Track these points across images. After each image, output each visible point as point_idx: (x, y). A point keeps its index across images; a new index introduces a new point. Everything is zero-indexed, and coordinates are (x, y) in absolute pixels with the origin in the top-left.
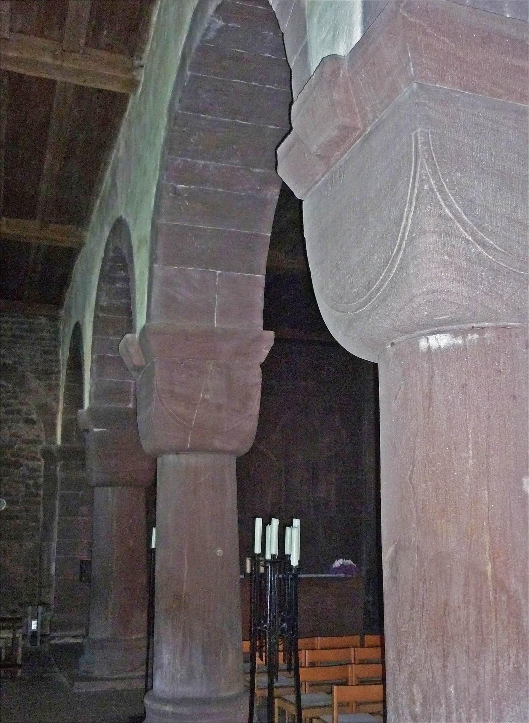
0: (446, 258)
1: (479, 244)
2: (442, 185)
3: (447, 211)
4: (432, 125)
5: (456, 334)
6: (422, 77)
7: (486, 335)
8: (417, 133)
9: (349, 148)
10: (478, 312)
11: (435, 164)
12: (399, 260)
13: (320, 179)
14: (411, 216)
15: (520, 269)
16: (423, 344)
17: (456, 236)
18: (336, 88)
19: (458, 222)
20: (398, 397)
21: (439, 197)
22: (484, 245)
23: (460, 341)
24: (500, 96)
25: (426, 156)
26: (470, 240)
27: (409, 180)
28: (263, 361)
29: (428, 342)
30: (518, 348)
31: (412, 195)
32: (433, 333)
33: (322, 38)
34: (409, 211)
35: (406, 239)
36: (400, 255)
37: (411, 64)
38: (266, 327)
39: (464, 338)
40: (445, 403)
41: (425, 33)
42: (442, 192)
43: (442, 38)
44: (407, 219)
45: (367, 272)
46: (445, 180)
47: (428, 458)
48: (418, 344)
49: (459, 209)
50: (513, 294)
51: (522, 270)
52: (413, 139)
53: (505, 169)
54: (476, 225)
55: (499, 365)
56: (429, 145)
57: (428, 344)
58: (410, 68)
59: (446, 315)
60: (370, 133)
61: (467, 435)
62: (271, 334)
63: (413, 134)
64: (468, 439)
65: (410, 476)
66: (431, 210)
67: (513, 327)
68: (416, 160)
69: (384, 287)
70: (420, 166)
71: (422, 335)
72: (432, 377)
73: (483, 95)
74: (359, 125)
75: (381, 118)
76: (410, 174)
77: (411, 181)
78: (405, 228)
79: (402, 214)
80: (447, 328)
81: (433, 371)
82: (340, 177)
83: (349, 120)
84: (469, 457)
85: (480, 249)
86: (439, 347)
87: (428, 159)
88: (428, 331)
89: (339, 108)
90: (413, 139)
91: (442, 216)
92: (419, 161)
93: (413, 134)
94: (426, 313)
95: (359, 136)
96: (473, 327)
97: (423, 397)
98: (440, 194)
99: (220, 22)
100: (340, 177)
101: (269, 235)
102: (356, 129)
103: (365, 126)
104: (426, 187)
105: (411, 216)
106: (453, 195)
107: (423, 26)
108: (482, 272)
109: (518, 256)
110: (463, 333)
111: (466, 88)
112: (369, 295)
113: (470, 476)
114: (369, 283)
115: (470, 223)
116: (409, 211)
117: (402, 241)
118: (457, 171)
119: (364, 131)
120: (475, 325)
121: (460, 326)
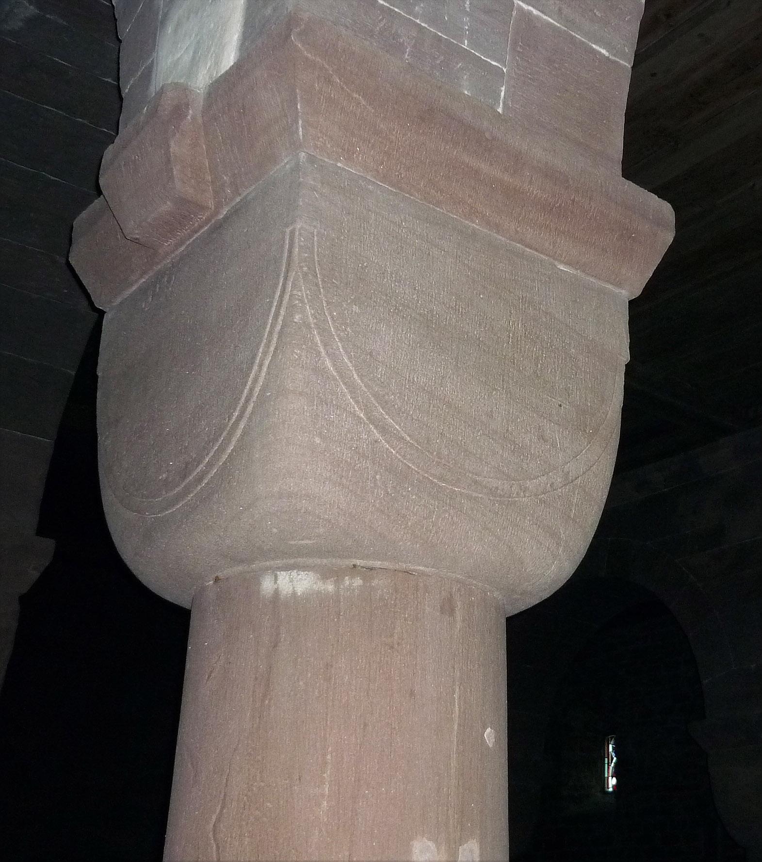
0: (318, 440)
1: (376, 427)
2: (325, 321)
3: (328, 363)
4: (321, 221)
5: (326, 574)
6: (316, 147)
7: (375, 583)
8: (294, 229)
9: (190, 236)
10: (364, 542)
11: (317, 285)
12: (239, 432)
13: (136, 281)
14: (267, 363)
15: (441, 478)
16: (267, 585)
17: (338, 407)
18: (177, 135)
19: (345, 384)
20: (213, 675)
21: (318, 339)
22: (384, 430)
23: (330, 587)
24: (438, 204)
25: (305, 269)
26: (361, 418)
27: (271, 302)
28: (24, 589)
29: (275, 583)
30: (428, 609)
31: (273, 326)
32: (288, 568)
33: (175, 58)
34: (265, 353)
35: (254, 399)
36: (242, 425)
37: (300, 122)
38: (41, 531)
39: (337, 582)
40: (292, 693)
41: (329, 81)
42: (323, 330)
43: (355, 95)
44: (261, 366)
45: (186, 447)
46: (331, 314)
47: (250, 793)
48: (259, 584)
49: (350, 364)
50: (425, 518)
51: (444, 481)
52: (287, 237)
53: (432, 316)
54: (374, 395)
55: (392, 636)
56: (312, 253)
57: (276, 586)
58: (297, 129)
59: (310, 539)
60: (226, 218)
61: (324, 755)
62: (49, 545)
63: (288, 230)
64: (325, 763)
65: (214, 825)
66: (300, 356)
67: (423, 574)
68: (287, 271)
69: (209, 476)
70: (293, 283)
71: (267, 569)
72: (275, 646)
73: (411, 195)
74: (211, 204)
75: (246, 197)
76: (274, 293)
77: (275, 304)
78: (255, 380)
79: (254, 357)
80: (310, 561)
81: (278, 634)
82: (169, 282)
83: (191, 191)
84: (323, 796)
85: (377, 435)
86: (294, 593)
87: (305, 275)
88: (279, 562)
89: (178, 167)
90: (287, 237)
91: (320, 371)
92: (292, 275)
93: (288, 230)
94: (275, 530)
95: (208, 220)
96: (355, 566)
97: (256, 679)
98: (319, 333)
99: (31, 7)
100: (169, 282)
101: (73, 373)
102: (203, 208)
103: (219, 206)
104: (297, 318)
105: (267, 363)
106: (341, 340)
107: (326, 70)
108: (376, 473)
109: (439, 455)
110: (337, 574)
111: (384, 179)
112: (185, 486)
113: (320, 831)
114: (186, 467)
115: (364, 388)
116: (265, 353)
117: (247, 400)
118: (354, 301)
119: (217, 212)
120: (358, 562)
121: (334, 560)
